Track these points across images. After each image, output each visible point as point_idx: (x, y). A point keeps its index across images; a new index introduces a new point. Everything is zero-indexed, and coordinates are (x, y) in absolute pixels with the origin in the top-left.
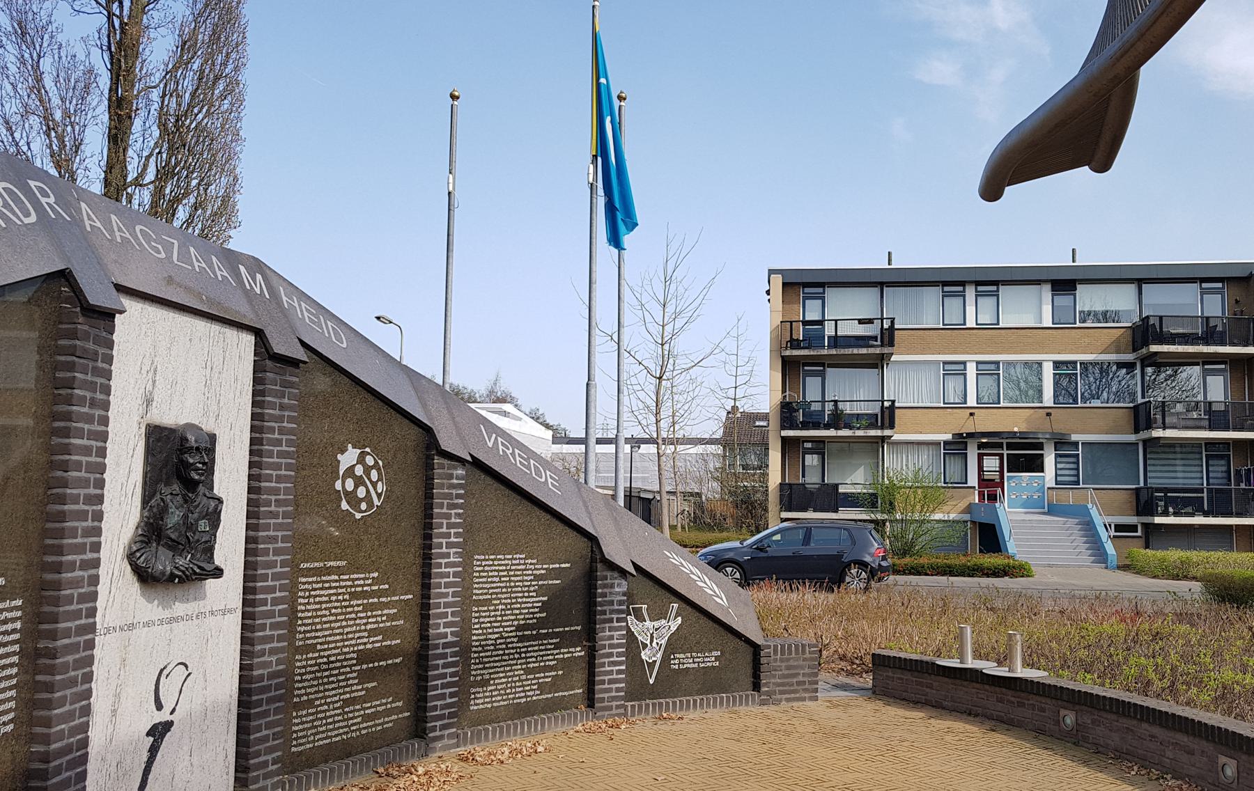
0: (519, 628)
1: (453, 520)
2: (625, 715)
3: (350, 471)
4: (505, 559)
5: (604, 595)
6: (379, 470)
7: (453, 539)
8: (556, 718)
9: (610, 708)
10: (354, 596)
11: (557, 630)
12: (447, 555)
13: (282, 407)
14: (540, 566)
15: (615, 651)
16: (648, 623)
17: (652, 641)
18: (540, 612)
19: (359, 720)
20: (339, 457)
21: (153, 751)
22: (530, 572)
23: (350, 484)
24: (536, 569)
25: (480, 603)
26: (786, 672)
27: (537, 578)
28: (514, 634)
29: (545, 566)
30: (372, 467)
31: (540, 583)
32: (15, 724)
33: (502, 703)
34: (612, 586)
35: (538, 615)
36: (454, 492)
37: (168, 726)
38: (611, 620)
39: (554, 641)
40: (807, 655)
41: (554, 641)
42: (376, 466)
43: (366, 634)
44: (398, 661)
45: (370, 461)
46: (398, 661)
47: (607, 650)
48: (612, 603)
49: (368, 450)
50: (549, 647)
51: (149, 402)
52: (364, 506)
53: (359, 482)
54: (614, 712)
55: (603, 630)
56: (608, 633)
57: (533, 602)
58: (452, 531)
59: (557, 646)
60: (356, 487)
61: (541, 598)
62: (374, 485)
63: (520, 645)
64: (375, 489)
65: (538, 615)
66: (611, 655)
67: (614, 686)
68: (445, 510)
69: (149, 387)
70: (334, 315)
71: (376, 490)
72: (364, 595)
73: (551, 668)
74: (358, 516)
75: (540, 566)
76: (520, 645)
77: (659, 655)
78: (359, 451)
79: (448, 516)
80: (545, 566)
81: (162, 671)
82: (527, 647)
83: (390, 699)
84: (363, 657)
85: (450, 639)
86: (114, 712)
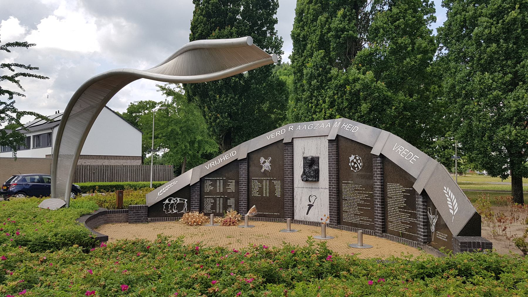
0: (399, 208)
1: (378, 172)
3: (353, 161)
6: (360, 160)
10: (355, 190)
11: (409, 211)
12: (377, 182)
13: (288, 155)
14: (403, 188)
18: (404, 204)
19: (359, 220)
20: (350, 158)
22: (401, 190)
23: (353, 164)
24: (402, 189)
25: (390, 198)
27: (403, 192)
28: (398, 209)
29: (405, 188)
30: (358, 160)
31: (404, 194)
32: (12, 148)
33: (396, 230)
35: (404, 205)
36: (378, 164)
37: (313, 205)
39: (409, 215)
41: (409, 215)
42: (359, 159)
43: (359, 199)
44: (369, 208)
45: (358, 158)
46: (369, 208)
49: (357, 155)
50: (407, 216)
51: (304, 153)
52: (357, 169)
53: (355, 163)
57: (402, 200)
58: (378, 175)
60: (354, 164)
61: (404, 199)
62: (359, 164)
63: (399, 213)
64: (359, 165)
65: (404, 205)
69: (304, 151)
70: (273, 143)
71: (360, 165)
72: (358, 190)
74: (355, 171)
75: (403, 188)
76: (399, 213)
78: (264, 160)
79: (376, 171)
80: (405, 188)
81: (310, 196)
82: (402, 214)
83: (368, 218)
86: (301, 200)
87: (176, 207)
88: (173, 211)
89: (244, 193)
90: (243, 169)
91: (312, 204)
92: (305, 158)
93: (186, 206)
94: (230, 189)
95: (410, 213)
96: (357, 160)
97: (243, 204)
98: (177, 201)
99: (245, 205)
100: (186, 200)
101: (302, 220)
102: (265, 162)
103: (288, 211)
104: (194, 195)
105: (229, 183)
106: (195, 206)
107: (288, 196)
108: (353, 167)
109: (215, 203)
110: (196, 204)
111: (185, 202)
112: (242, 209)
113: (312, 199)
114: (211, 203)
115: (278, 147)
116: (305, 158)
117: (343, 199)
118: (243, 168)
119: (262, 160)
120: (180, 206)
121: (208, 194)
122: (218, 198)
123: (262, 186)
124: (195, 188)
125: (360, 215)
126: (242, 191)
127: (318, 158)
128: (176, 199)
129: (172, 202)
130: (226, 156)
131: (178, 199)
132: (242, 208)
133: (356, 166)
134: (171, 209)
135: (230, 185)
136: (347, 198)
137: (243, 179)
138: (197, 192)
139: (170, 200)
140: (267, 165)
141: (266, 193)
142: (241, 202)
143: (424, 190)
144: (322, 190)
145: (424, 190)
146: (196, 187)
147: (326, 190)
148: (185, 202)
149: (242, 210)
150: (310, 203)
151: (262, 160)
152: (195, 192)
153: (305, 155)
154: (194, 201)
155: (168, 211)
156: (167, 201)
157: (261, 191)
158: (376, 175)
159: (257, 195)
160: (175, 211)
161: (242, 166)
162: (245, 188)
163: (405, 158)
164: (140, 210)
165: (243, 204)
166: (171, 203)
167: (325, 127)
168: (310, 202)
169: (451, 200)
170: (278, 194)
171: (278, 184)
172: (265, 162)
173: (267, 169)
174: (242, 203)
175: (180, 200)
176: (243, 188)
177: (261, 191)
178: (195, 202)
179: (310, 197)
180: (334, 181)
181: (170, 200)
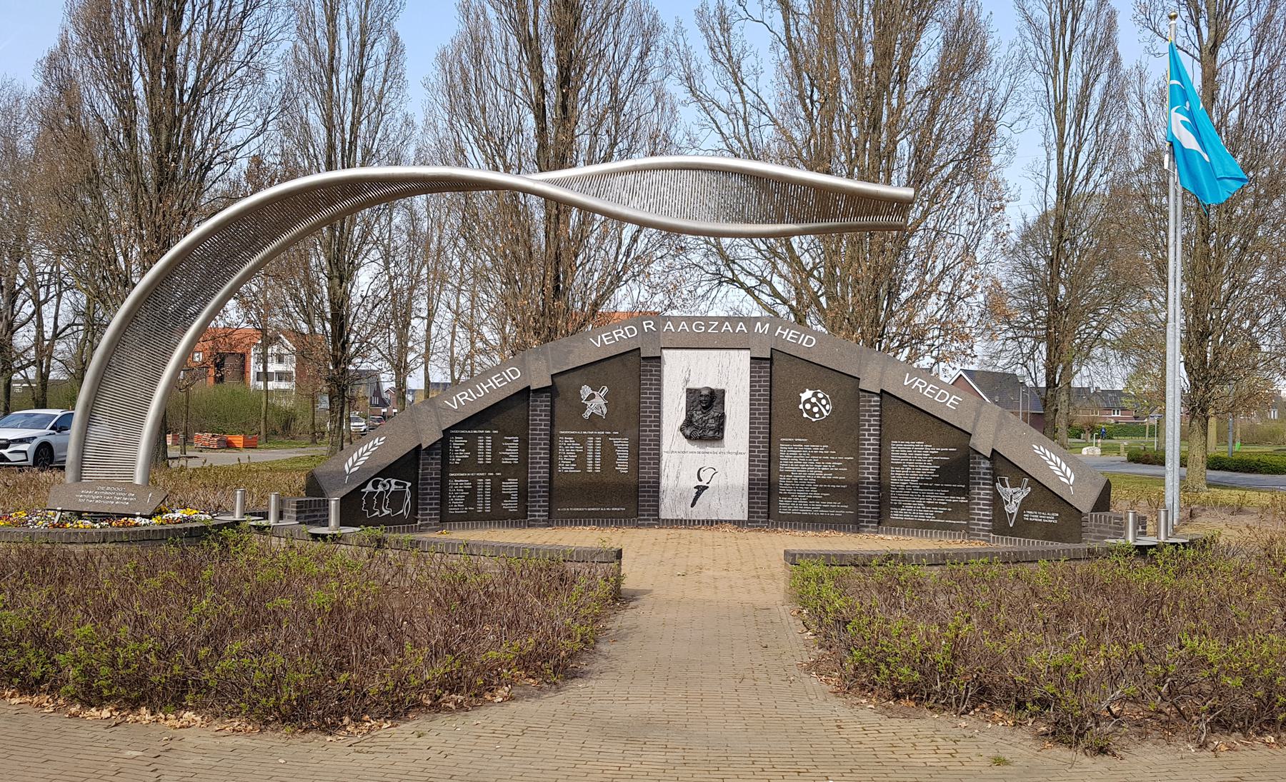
0: (920, 481)
2: (989, 541)
3: (808, 401)
4: (910, 444)
5: (974, 468)
6: (827, 399)
7: (872, 432)
8: (945, 534)
9: (979, 535)
13: (650, 384)
15: (982, 502)
16: (1009, 489)
17: (1011, 501)
20: (801, 395)
21: (698, 495)
26: (1098, 534)
34: (979, 463)
38: (979, 484)
40: (1112, 525)
42: (825, 397)
45: (820, 395)
47: (976, 501)
48: (979, 473)
51: (687, 381)
52: (817, 416)
54: (981, 538)
55: (974, 488)
56: (977, 491)
59: (946, 494)
60: (812, 407)
66: (979, 504)
67: (981, 523)
68: (867, 418)
69: (687, 376)
72: (819, 454)
73: (943, 506)
74: (814, 420)
77: (1016, 509)
78: (592, 392)
79: (869, 421)
81: (699, 472)
84: (819, 481)
85: (871, 480)
86: (677, 477)
87: (388, 502)
88: (382, 512)
89: (542, 465)
90: (541, 411)
91: (705, 484)
92: (690, 392)
93: (409, 498)
94: (507, 456)
95: (947, 488)
96: (819, 400)
97: (540, 492)
98: (390, 485)
99: (544, 492)
100: (409, 484)
101: (680, 518)
102: (592, 397)
103: (649, 501)
104: (429, 471)
105: (506, 444)
106: (431, 499)
107: (646, 473)
108: (810, 412)
109: (473, 491)
110: (434, 492)
111: (407, 490)
112: (539, 501)
113: (705, 477)
114: (465, 490)
115: (624, 365)
116: (690, 392)
117: (781, 473)
118: (540, 407)
119: (586, 391)
120: (397, 498)
121: (458, 468)
122: (481, 477)
123: (585, 449)
124: (432, 455)
125: (820, 500)
126: (538, 460)
127: (723, 392)
128: (389, 482)
129: (380, 489)
130: (931, 388)
131: (393, 481)
132: (538, 499)
133: (815, 409)
134: (378, 506)
135: (507, 447)
136: (788, 469)
137: (541, 435)
138: (436, 464)
139: (375, 485)
140: (597, 404)
141: (594, 465)
142: (873, 468)
143: (994, 450)
144: (729, 456)
145: (994, 450)
146: (434, 452)
147: (739, 456)
148: (407, 490)
149: (538, 504)
150: (700, 483)
151: (586, 391)
152: (431, 464)
153: (691, 386)
154: (429, 487)
155: (372, 512)
156: (370, 488)
157: (581, 460)
158: (867, 427)
159: (571, 469)
160: (386, 512)
161: (538, 403)
162: (544, 454)
163: (936, 399)
164: (317, 510)
165: (540, 492)
166: (378, 491)
167: (734, 331)
168: (700, 480)
169: (1056, 464)
170: (622, 466)
171: (622, 446)
172: (592, 397)
173: (598, 412)
174: (538, 489)
175: (396, 483)
176: (539, 453)
177: (581, 460)
178: (431, 489)
179: (701, 471)
180: (762, 438)
181: (375, 485)
